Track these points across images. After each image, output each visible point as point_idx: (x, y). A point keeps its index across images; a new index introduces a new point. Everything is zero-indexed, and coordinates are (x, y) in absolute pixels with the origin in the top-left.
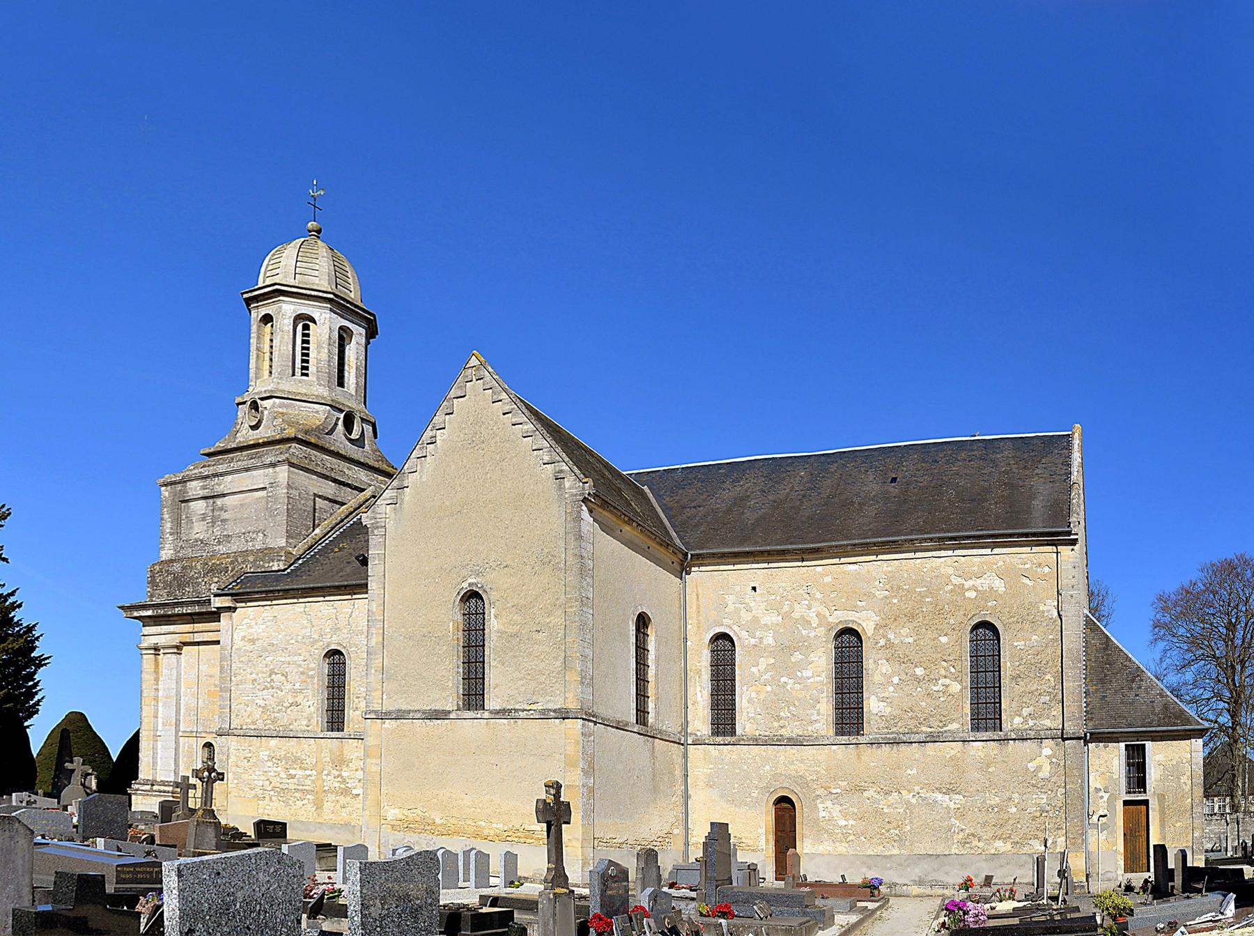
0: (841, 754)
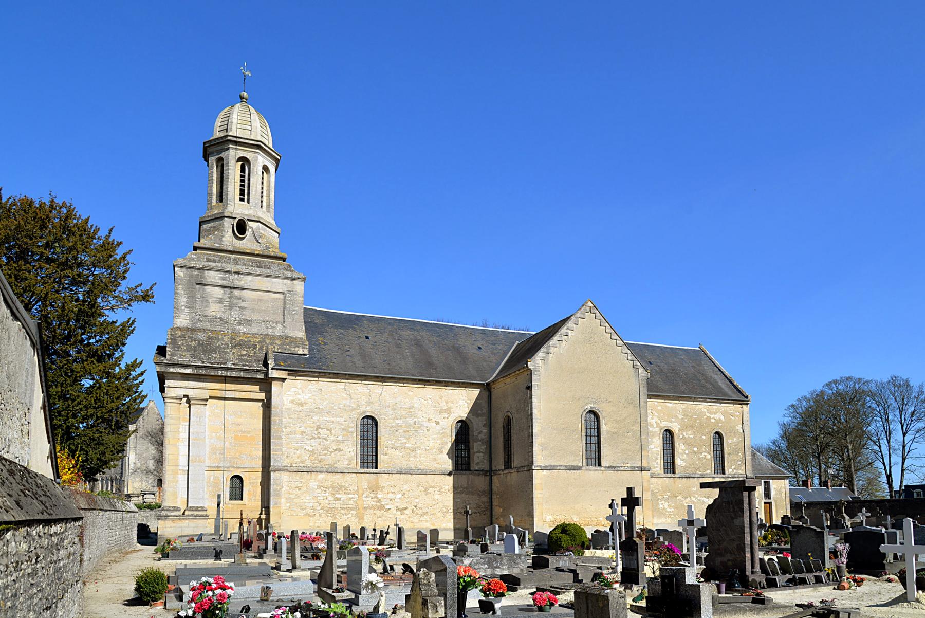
0: (667, 481)
